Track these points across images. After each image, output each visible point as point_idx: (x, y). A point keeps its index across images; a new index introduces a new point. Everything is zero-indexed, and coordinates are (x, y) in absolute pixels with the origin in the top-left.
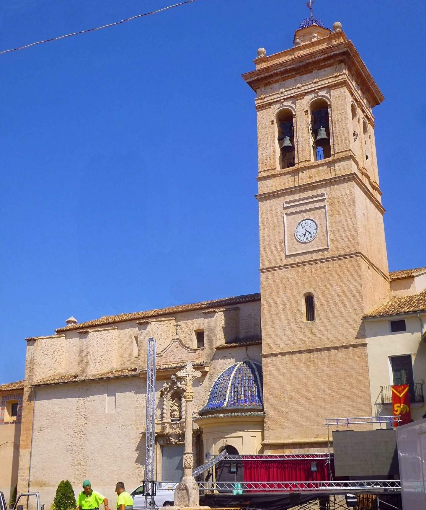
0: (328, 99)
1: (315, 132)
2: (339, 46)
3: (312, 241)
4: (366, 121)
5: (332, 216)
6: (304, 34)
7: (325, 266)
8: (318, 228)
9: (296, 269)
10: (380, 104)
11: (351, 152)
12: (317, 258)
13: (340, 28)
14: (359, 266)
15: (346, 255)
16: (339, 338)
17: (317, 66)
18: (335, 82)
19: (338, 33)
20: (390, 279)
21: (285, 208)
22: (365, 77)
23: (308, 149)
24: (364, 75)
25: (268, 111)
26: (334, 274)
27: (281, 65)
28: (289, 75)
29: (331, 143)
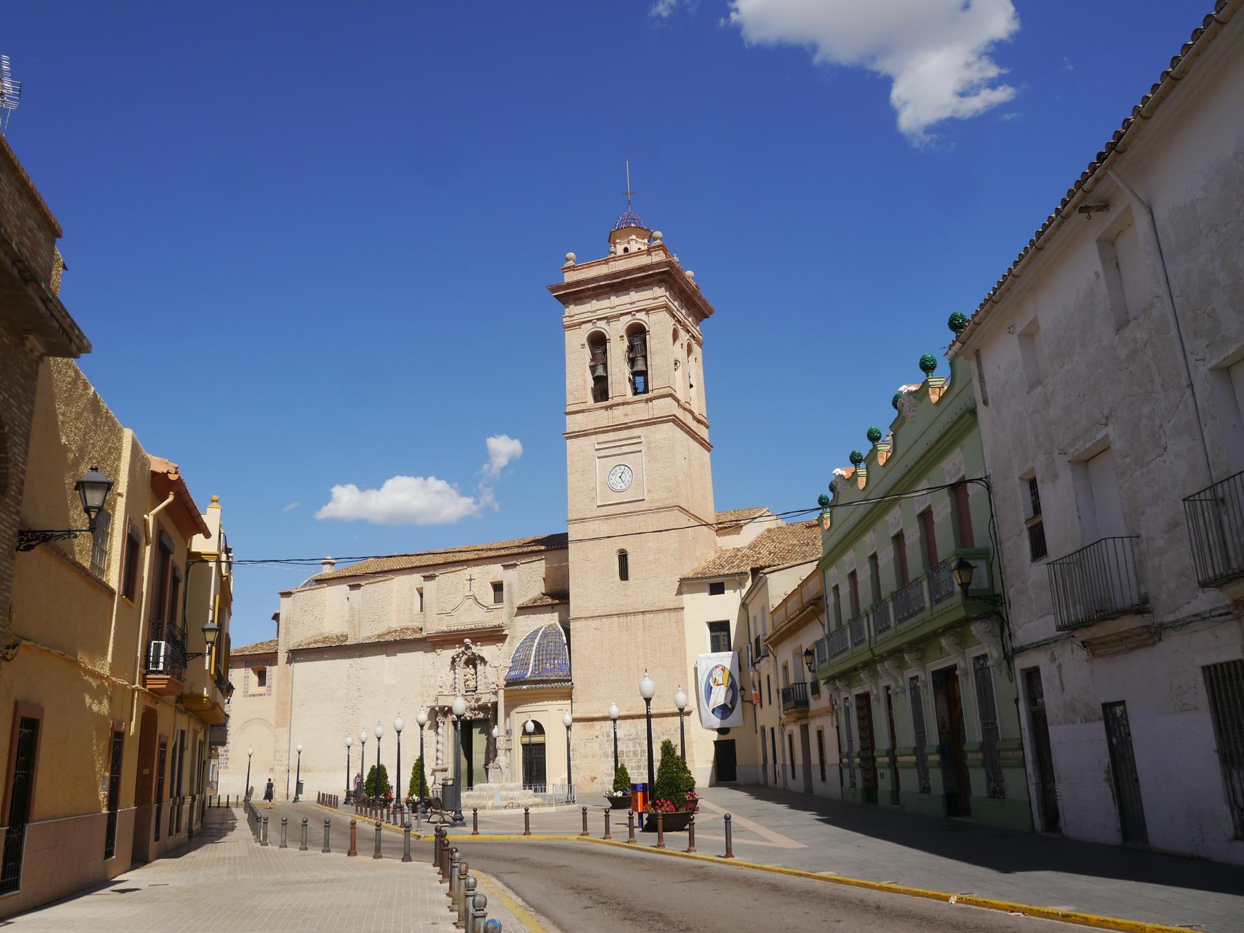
1: (632, 362)
9: (608, 521)
10: (708, 317)
13: (661, 239)
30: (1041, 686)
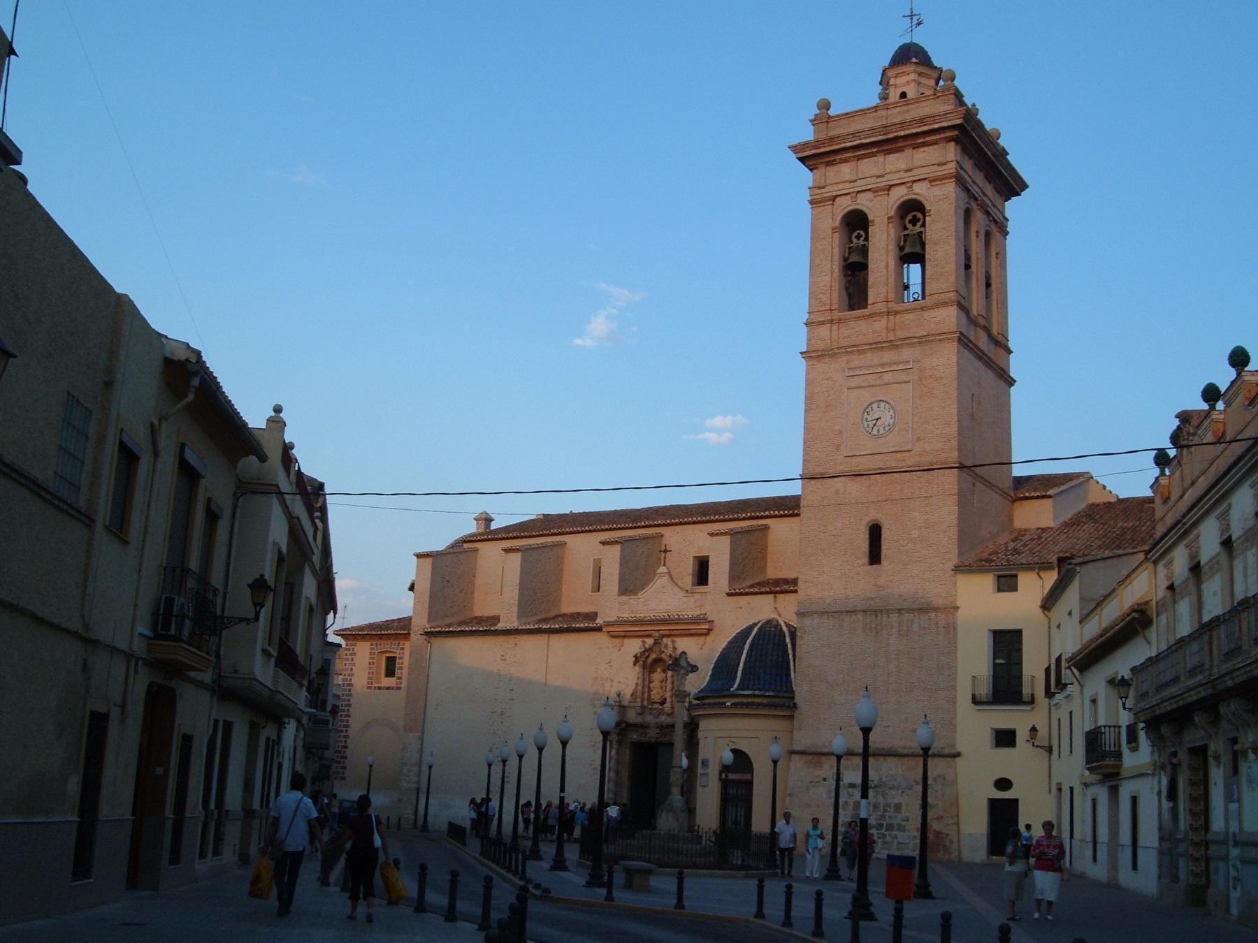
7: (903, 478)
30: (393, 621)
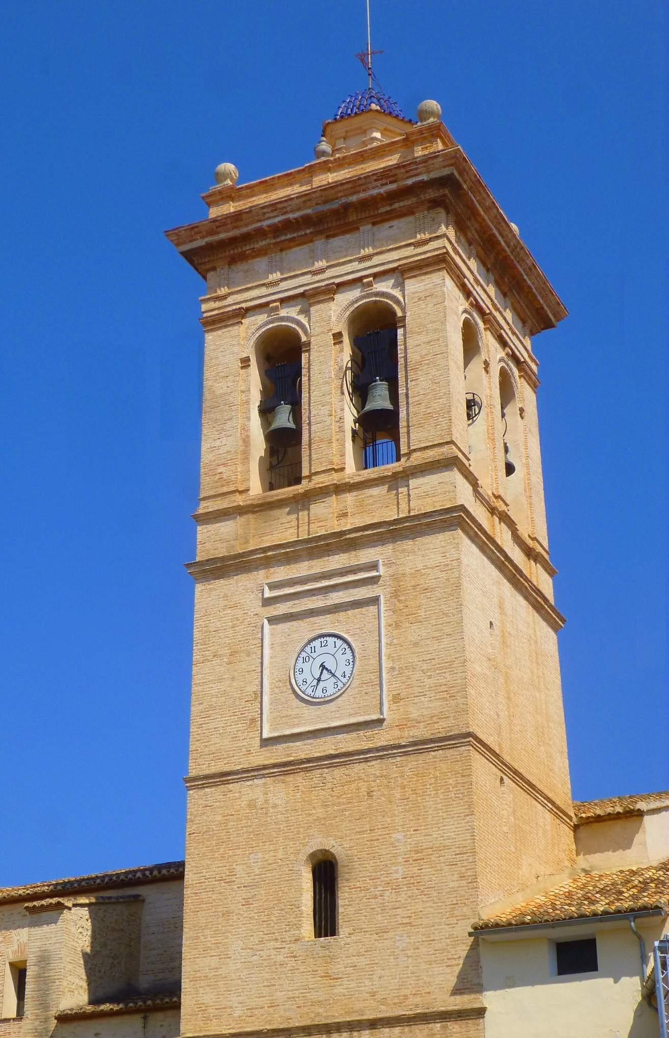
0: (397, 302)
1: (361, 391)
2: (430, 162)
3: (337, 698)
4: (511, 370)
5: (397, 626)
6: (347, 132)
7: (372, 771)
8: (357, 663)
9: (289, 778)
10: (553, 326)
11: (454, 447)
12: (351, 749)
13: (439, 117)
14: (466, 773)
15: (431, 741)
16: (407, 992)
17: (372, 213)
18: (419, 258)
19: (430, 128)
20: (575, 819)
21: (267, 602)
22: (507, 249)
23: (338, 437)
24: (503, 243)
25: (236, 331)
26: (398, 796)
27: (271, 208)
28: (295, 235)
29: (402, 423)
